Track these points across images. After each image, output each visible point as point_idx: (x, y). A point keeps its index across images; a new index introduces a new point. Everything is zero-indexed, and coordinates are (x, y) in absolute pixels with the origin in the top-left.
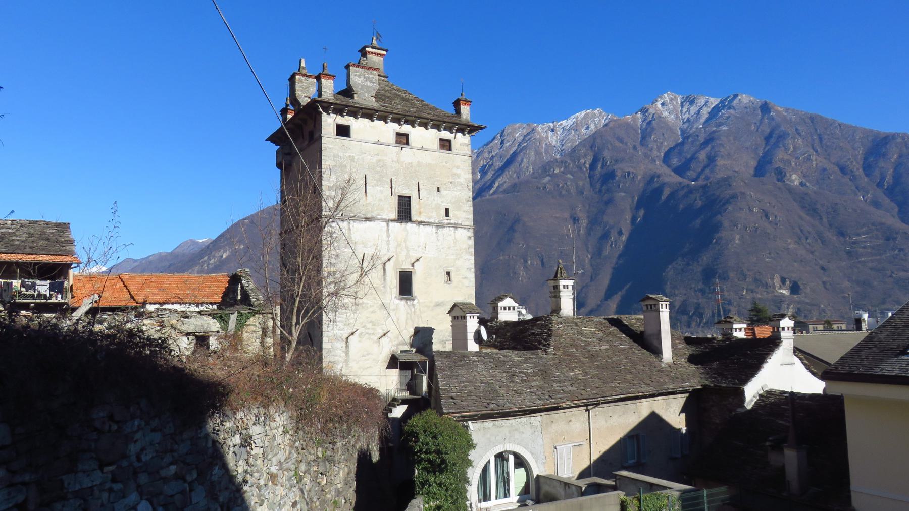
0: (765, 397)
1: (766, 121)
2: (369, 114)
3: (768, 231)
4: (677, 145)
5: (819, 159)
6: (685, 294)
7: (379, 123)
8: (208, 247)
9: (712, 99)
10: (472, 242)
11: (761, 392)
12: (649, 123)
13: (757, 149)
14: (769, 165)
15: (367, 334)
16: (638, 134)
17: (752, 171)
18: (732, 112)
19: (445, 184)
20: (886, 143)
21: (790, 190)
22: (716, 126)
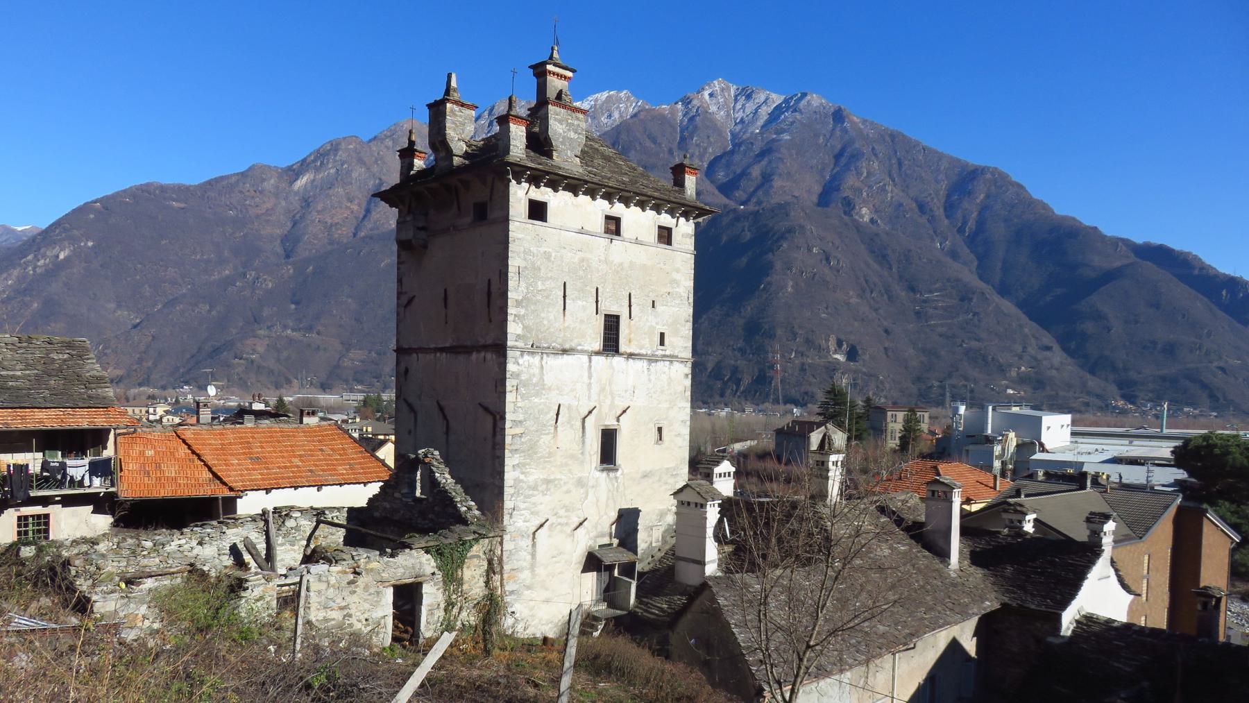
0: (1086, 625)
1: (838, 133)
2: (574, 186)
3: (828, 279)
4: (725, 154)
5: (896, 191)
6: (721, 354)
7: (584, 199)
8: (34, 239)
9: (773, 95)
10: (688, 382)
11: (1077, 617)
12: (692, 119)
13: (824, 169)
14: (836, 193)
15: (559, 524)
16: (676, 132)
17: (815, 199)
18: (798, 115)
19: (662, 296)
20: (974, 179)
21: (858, 227)
22: (776, 133)
